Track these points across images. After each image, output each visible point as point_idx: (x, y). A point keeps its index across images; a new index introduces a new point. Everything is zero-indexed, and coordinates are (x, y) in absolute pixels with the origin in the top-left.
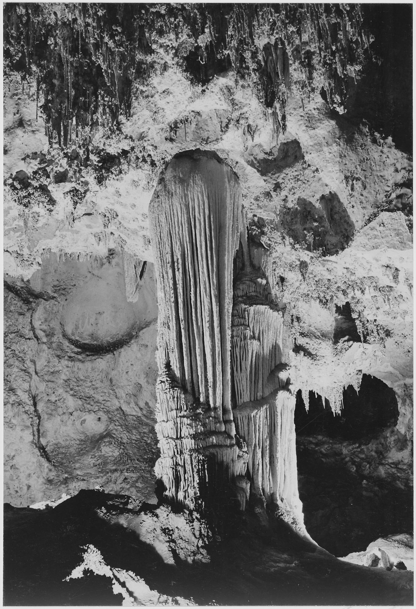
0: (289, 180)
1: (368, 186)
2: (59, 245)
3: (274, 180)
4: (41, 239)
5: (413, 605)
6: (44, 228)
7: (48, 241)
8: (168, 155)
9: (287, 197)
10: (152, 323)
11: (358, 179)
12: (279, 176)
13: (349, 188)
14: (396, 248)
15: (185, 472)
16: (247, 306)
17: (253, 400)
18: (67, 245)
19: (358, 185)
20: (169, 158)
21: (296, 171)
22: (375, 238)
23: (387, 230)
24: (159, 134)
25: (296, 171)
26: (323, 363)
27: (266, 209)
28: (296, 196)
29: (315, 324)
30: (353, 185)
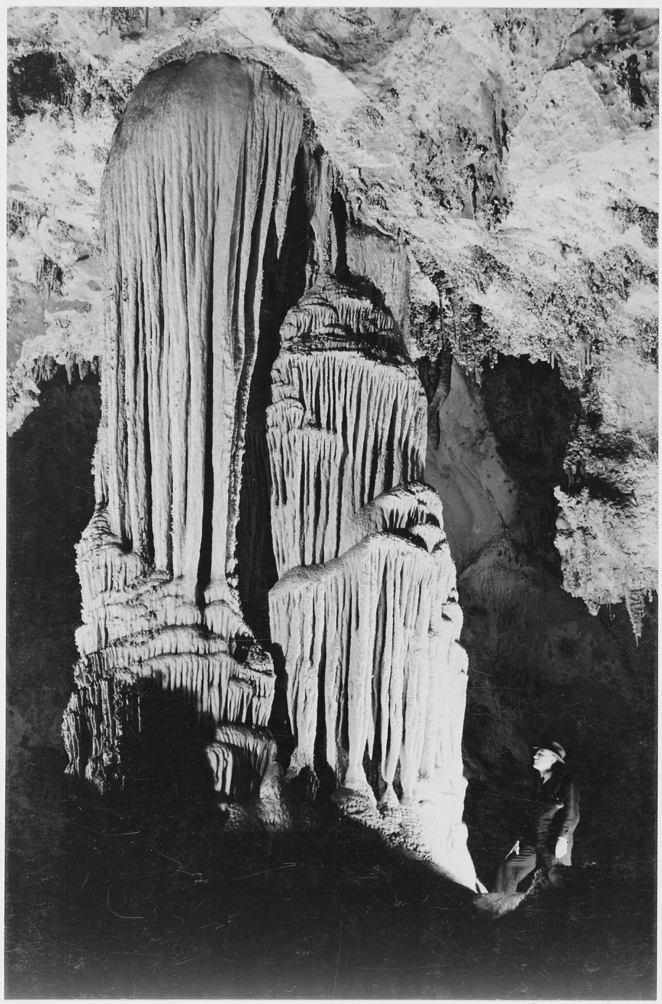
1: (544, 32)
2: (65, 346)
3: (378, 76)
6: (19, 310)
7: (39, 339)
8: (135, 71)
13: (507, 47)
14: (586, 150)
15: (100, 720)
16: (295, 356)
17: (308, 561)
18: (79, 342)
23: (563, 113)
24: (87, 26)
26: (648, 511)
28: (433, 103)
29: (641, 427)
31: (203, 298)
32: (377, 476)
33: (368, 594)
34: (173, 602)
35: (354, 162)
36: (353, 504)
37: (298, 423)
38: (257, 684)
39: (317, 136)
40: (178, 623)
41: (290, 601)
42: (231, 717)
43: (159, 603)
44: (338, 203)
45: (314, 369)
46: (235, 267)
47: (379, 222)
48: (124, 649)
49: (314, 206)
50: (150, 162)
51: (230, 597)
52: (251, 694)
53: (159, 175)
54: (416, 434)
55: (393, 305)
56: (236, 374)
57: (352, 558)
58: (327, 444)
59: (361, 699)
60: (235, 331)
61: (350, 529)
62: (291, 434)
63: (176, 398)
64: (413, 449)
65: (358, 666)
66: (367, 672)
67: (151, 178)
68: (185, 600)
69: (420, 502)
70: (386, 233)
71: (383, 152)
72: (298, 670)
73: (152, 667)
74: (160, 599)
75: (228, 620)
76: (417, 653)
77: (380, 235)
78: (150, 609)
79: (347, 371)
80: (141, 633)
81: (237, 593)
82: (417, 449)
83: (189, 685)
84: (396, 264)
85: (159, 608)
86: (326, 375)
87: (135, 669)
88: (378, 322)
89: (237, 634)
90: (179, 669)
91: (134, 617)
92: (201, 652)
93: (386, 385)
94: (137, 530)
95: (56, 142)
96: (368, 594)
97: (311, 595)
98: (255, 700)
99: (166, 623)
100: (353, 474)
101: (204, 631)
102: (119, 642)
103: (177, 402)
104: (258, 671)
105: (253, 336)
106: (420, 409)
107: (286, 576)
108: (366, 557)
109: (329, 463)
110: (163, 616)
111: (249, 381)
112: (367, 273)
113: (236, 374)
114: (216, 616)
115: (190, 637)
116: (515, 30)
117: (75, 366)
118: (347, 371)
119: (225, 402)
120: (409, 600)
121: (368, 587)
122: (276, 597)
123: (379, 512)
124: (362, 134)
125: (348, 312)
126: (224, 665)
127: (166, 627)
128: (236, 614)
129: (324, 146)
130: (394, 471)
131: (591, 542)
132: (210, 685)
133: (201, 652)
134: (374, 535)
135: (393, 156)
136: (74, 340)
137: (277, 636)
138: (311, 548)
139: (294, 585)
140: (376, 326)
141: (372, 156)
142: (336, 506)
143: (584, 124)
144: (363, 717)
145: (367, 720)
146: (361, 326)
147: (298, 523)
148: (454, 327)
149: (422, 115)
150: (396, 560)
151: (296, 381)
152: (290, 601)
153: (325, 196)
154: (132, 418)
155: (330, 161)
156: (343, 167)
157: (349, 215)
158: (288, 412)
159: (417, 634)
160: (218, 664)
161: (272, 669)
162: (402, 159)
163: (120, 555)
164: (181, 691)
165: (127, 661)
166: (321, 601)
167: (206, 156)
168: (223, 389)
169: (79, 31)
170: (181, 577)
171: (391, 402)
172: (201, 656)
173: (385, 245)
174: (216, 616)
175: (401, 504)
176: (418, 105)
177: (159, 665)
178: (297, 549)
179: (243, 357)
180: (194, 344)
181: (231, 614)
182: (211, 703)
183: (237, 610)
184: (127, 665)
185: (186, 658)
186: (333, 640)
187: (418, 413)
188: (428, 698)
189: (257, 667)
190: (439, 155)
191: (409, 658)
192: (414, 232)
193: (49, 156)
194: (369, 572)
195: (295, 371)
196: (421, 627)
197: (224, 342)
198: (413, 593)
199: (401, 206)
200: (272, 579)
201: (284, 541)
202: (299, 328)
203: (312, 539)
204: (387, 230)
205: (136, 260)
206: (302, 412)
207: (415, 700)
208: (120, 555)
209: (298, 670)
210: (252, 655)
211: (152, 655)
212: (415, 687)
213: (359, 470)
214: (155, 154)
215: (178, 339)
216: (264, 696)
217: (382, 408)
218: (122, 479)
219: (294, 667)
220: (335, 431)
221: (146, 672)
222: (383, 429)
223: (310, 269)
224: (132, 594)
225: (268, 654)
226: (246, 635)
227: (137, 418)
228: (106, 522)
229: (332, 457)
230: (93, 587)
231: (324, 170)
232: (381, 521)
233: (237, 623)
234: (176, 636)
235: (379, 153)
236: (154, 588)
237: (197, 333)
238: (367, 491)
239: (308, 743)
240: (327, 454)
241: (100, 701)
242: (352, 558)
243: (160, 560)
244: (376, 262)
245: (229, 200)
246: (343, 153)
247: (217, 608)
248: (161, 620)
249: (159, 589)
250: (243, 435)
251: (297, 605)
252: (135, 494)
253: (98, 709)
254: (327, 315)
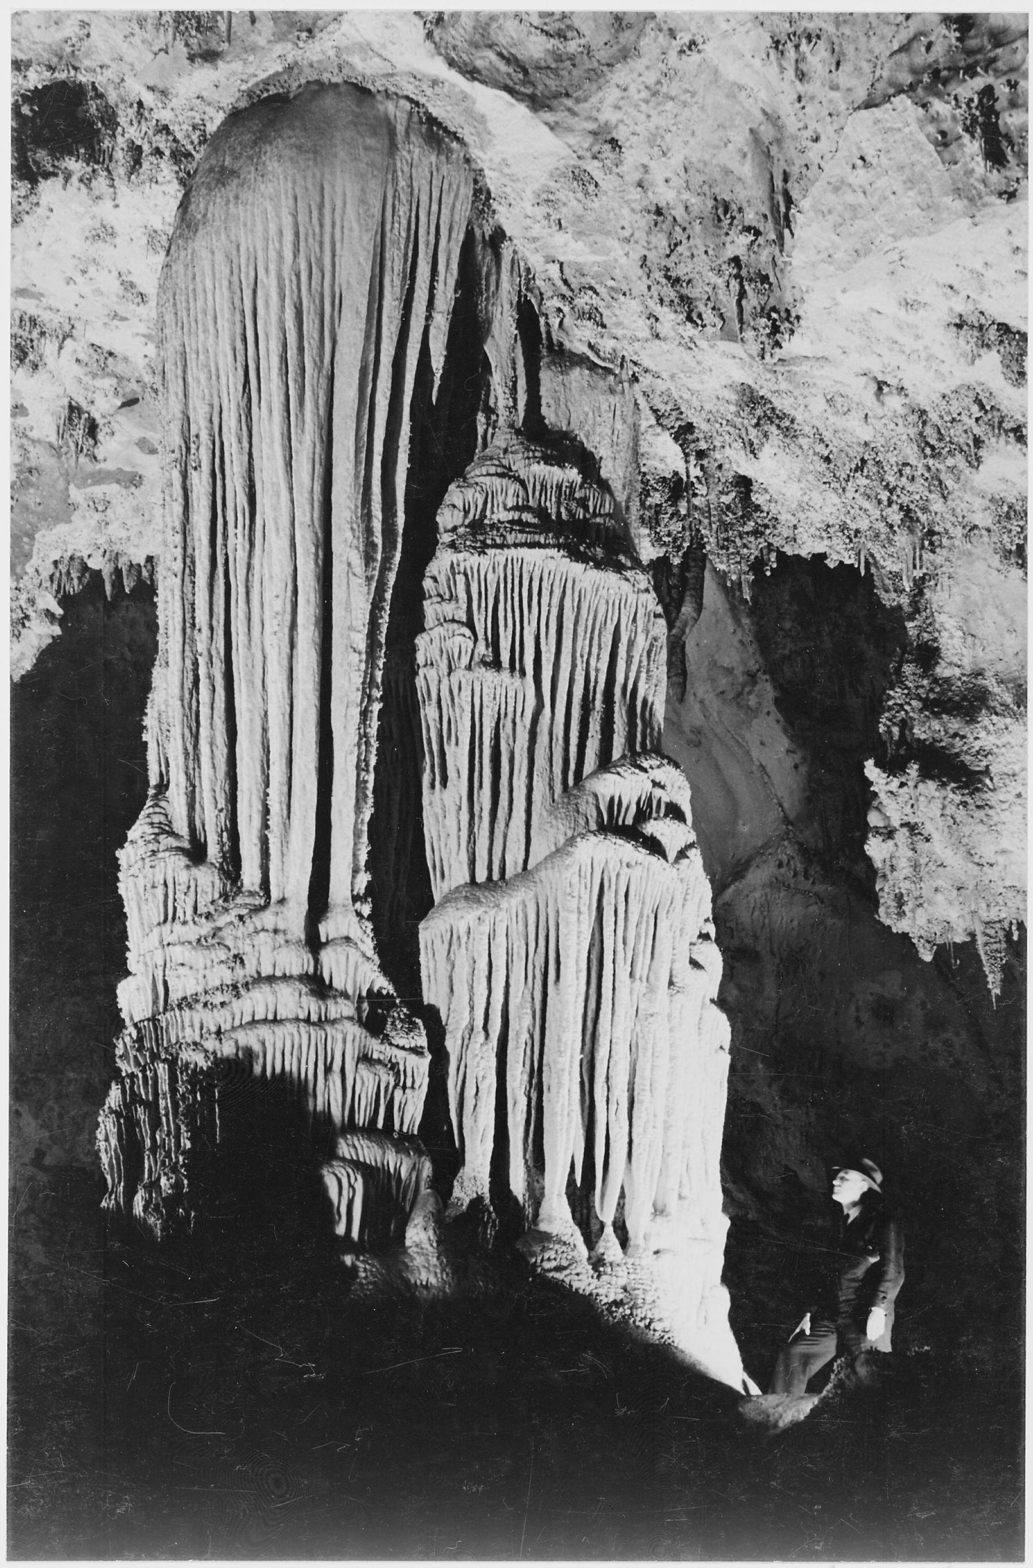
1: (849, 50)
2: (102, 540)
3: (589, 118)
5: (1022, 1559)
6: (29, 484)
8: (211, 111)
9: (646, 168)
10: (754, 864)
13: (790, 73)
14: (914, 235)
15: (155, 1124)
16: (461, 556)
17: (481, 876)
18: (123, 534)
20: (215, 121)
22: (854, 218)
26: (1011, 797)
27: (582, 227)
28: (676, 160)
29: (1000, 667)
31: (317, 466)
32: (589, 743)
33: (574, 928)
34: (269, 940)
35: (553, 252)
36: (551, 788)
37: (465, 660)
38: (402, 1068)
39: (494, 212)
40: (278, 974)
41: (452, 939)
42: (361, 1119)
43: (248, 941)
44: (528, 318)
45: (490, 576)
46: (367, 417)
48: (194, 1013)
49: (489, 322)
50: (235, 252)
51: (360, 933)
52: (392, 1083)
53: (248, 273)
54: (649, 678)
55: (614, 476)
56: (369, 585)
57: (550, 871)
58: (511, 694)
59: (564, 1092)
60: (367, 516)
61: (547, 827)
62: (455, 678)
63: (275, 622)
64: (645, 702)
65: (559, 1040)
66: (573, 1049)
67: (235, 278)
68: (289, 937)
69: (656, 784)
70: (603, 364)
71: (598, 238)
72: (464, 1046)
73: (236, 1042)
74: (249, 935)
75: (356, 968)
76: (651, 1020)
77: (593, 367)
78: (234, 951)
79: (541, 580)
80: (221, 988)
81: (370, 926)
82: (650, 700)
83: (295, 1070)
84: (618, 413)
85: (248, 949)
86: (509, 586)
87: (211, 1044)
88: (591, 504)
89: (370, 991)
90: (279, 1045)
91: (209, 963)
92: (314, 1018)
93: (603, 601)
94: (213, 827)
95: (87, 222)
96: (574, 928)
97: (486, 929)
98: (398, 1094)
99: (259, 973)
100: (551, 739)
101: (318, 985)
102: (187, 1003)
103: (276, 628)
104: (403, 1048)
105: (394, 524)
106: (655, 639)
107: (447, 900)
108: (571, 870)
109: (514, 723)
110: (255, 962)
111: (388, 596)
112: (572, 426)
113: (369, 585)
114: (338, 962)
115: (297, 994)
117: (118, 572)
118: (541, 580)
119: (351, 628)
120: (638, 936)
121: (574, 917)
122: (430, 933)
123: (591, 800)
124: (564, 210)
125: (544, 487)
126: (350, 1038)
127: (260, 979)
128: (368, 959)
129: (505, 228)
130: (615, 736)
131: (922, 846)
132: (328, 1070)
133: (314, 1018)
134: (583, 836)
135: (613, 243)
136: (115, 530)
137: (432, 994)
138: (486, 856)
139: (459, 913)
140: (586, 508)
141: (580, 244)
142: (524, 791)
143: (911, 193)
144: (566, 1119)
145: (573, 1125)
146: (563, 510)
147: (465, 817)
148: (709, 511)
149: (659, 179)
150: (618, 875)
151: (462, 596)
152: (452, 939)
153: (507, 306)
154: (205, 653)
155: (515, 252)
156: (536, 261)
157: (544, 336)
158: (449, 644)
159: (651, 990)
160: (340, 1037)
161: (425, 1044)
162: (627, 248)
163: (188, 867)
164: (282, 1078)
165: (197, 1032)
166: (501, 939)
167: (321, 244)
168: (348, 608)
169: (124, 48)
170: (282, 901)
171: (611, 628)
172: (314, 1024)
173: (601, 383)
174: (338, 962)
175: (625, 786)
176: (652, 164)
177: (249, 1039)
178: (464, 857)
179: (379, 557)
180: (303, 536)
181: (361, 960)
182: (329, 1097)
183: (371, 953)
184: (198, 1039)
185: (290, 1028)
186: (518, 1000)
187: (652, 645)
188: (668, 1090)
189: (402, 1042)
190: (684, 241)
191: (638, 1028)
192: (646, 363)
193: (76, 244)
194: (576, 894)
195: (460, 579)
196: (657, 979)
197: (349, 535)
198: (644, 925)
199: (626, 321)
200: (424, 905)
201: (443, 845)
202: (466, 512)
203: (487, 843)
204: (604, 360)
205: (212, 406)
206: (471, 644)
207: (648, 1093)
208: (188, 867)
209: (464, 1046)
210: (393, 1023)
211: (237, 1023)
212: (648, 1073)
213: (561, 734)
214: (242, 240)
215: (277, 530)
216: (413, 1087)
217: (596, 637)
218: (190, 749)
219: (460, 1042)
220: (523, 673)
221: (227, 1049)
222: (597, 670)
223: (483, 420)
224: (205, 928)
225: (419, 1021)
226: (384, 992)
227: (214, 653)
228: (166, 815)
229: (518, 714)
230: (145, 917)
231: (506, 265)
232: (595, 814)
233: (369, 973)
234: (274, 993)
235: (592, 238)
236: (241, 918)
237: (307, 519)
238: (572, 766)
239: (480, 1160)
240: (510, 709)
241: (156, 1094)
242: (550, 871)
243: (250, 875)
244: (586, 409)
245: (357, 312)
246: (535, 240)
247: (339, 949)
248: (250, 969)
249: (248, 921)
250: (379, 680)
251: (463, 945)
252: (211, 771)
253: (152, 1107)
254: (511, 492)
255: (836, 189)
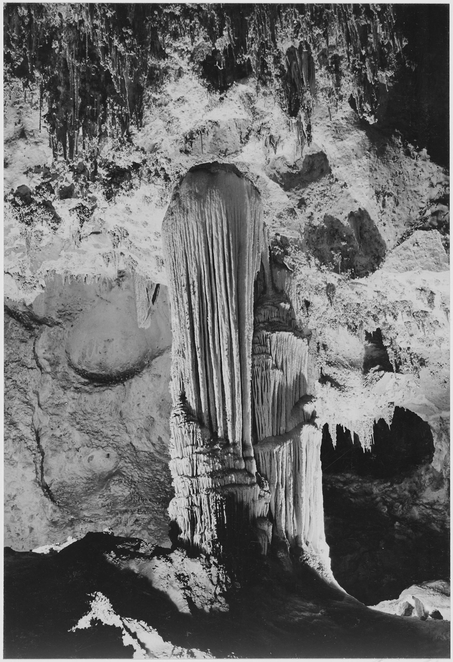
0: (315, 196)
2: (65, 267)
3: (299, 195)
4: (44, 260)
5: (449, 657)
6: (48, 247)
7: (53, 262)
8: (182, 169)
9: (312, 214)
10: (166, 352)
11: (390, 195)
12: (303, 192)
13: (381, 204)
14: (431, 270)
15: (201, 514)
16: (269, 333)
17: (275, 434)
18: (73, 266)
19: (390, 201)
20: (184, 172)
21: (322, 186)
22: (408, 259)
23: (421, 250)
24: (173, 146)
25: (322, 186)
26: (351, 394)
27: (290, 227)
28: (323, 213)
29: (343, 353)
30: (384, 201)
47: (419, 328)
116: (386, 198)
117: (66, 277)
131: (324, 404)
143: (432, 258)
169: (169, 148)
176: (315, 213)
255: (405, 249)
